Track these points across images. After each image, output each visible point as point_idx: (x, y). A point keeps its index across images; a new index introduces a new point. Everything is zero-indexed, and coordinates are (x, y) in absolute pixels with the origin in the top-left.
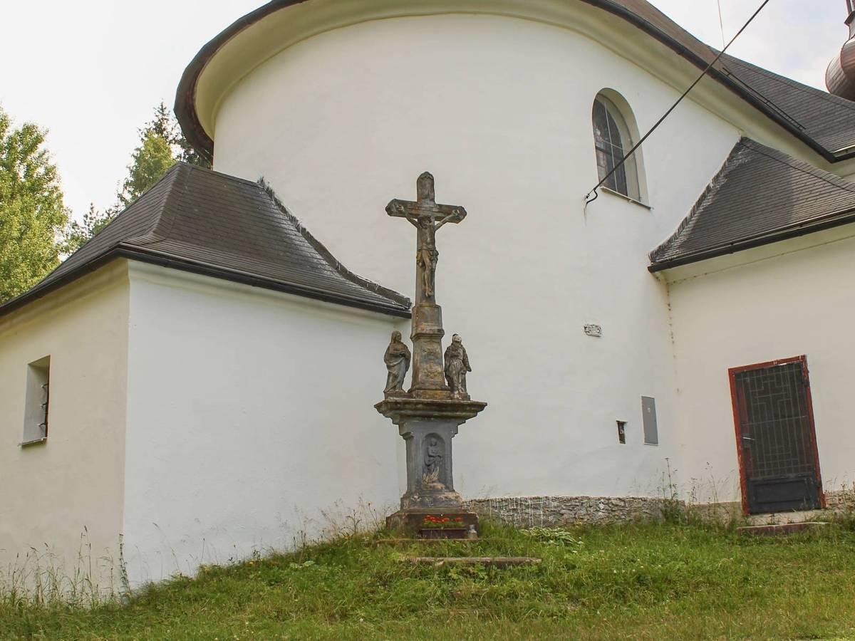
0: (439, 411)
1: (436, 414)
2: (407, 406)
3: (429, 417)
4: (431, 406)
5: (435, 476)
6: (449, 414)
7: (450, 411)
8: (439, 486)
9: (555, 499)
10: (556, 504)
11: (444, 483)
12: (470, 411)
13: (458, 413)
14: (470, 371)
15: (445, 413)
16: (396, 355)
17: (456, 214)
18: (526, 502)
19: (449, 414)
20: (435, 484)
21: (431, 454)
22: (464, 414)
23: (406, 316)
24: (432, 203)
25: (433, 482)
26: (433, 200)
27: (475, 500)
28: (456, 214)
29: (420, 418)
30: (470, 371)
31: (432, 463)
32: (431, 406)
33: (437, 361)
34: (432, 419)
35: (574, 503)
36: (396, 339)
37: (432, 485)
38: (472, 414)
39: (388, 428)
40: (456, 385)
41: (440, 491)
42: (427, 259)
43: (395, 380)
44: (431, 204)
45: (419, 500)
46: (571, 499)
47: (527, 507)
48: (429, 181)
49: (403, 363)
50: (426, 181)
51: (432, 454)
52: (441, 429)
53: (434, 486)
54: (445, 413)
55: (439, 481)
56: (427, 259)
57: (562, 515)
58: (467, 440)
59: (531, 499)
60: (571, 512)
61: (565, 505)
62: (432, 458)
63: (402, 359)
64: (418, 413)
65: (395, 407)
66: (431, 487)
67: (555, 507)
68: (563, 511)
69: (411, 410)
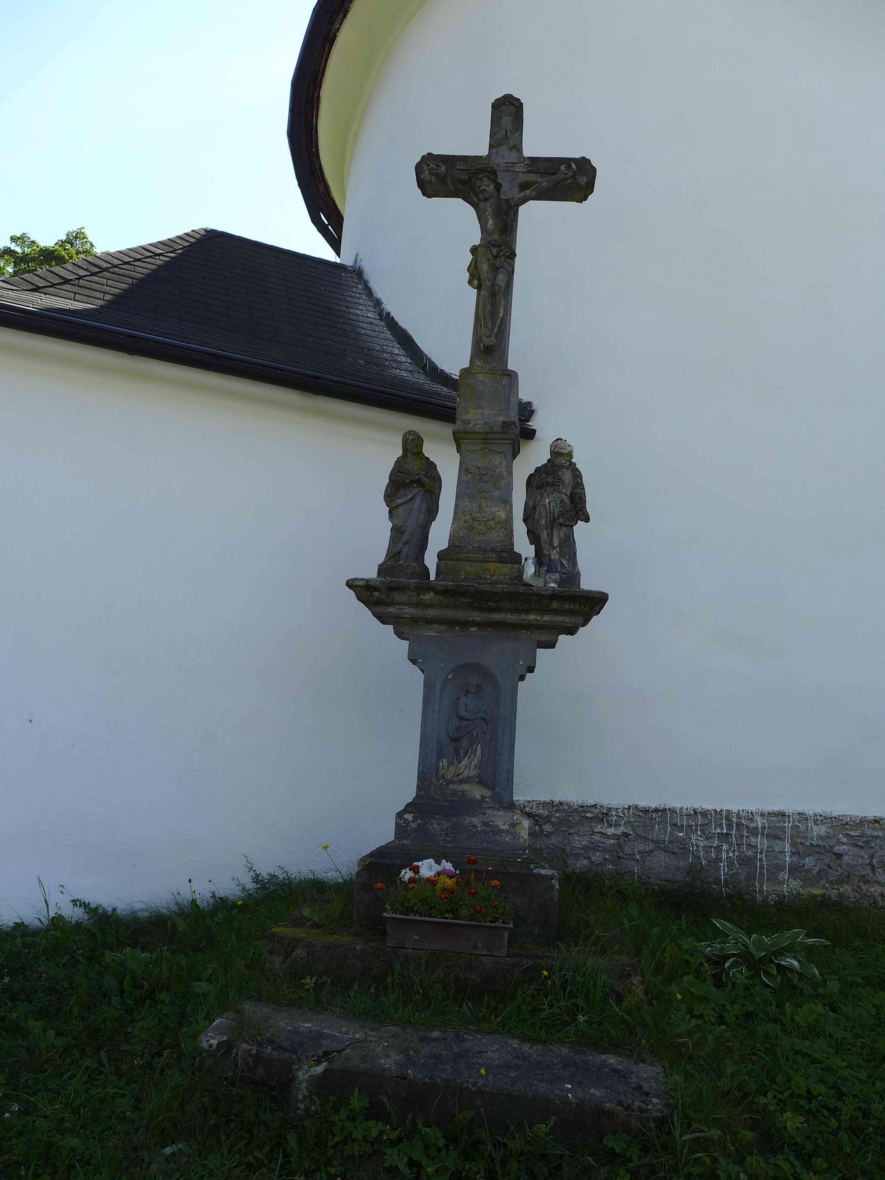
0: (481, 609)
1: (477, 616)
2: (397, 596)
3: (465, 624)
4: (485, 593)
5: (469, 766)
6: (511, 618)
7: (511, 611)
8: (477, 792)
9: (545, 804)
10: (823, 830)
11: (491, 786)
12: (570, 613)
13: (532, 617)
14: (587, 519)
15: (496, 616)
16: (411, 484)
17: (571, 180)
18: (752, 820)
19: (511, 618)
20: (466, 787)
21: (462, 713)
22: (546, 618)
23: (465, 407)
24: (514, 154)
25: (462, 782)
26: (518, 148)
27: (636, 807)
28: (571, 180)
29: (443, 627)
30: (587, 519)
31: (469, 728)
32: (485, 593)
33: (497, 493)
34: (473, 629)
35: (869, 832)
36: (412, 445)
37: (459, 788)
38: (567, 620)
39: (387, 645)
40: (546, 552)
41: (473, 806)
42: (493, 266)
43: (408, 540)
44: (513, 157)
45: (414, 825)
46: (863, 822)
47: (754, 832)
48: (512, 109)
49: (418, 500)
50: (508, 112)
51: (467, 715)
52: (494, 653)
53: (463, 792)
54: (496, 616)
55: (481, 781)
56: (493, 266)
57: (839, 856)
58: (560, 679)
59: (763, 815)
60: (862, 853)
61: (847, 835)
62: (465, 723)
63: (417, 490)
64: (431, 613)
65: (387, 593)
66: (454, 793)
67: (820, 837)
68: (838, 849)
69: (411, 605)
